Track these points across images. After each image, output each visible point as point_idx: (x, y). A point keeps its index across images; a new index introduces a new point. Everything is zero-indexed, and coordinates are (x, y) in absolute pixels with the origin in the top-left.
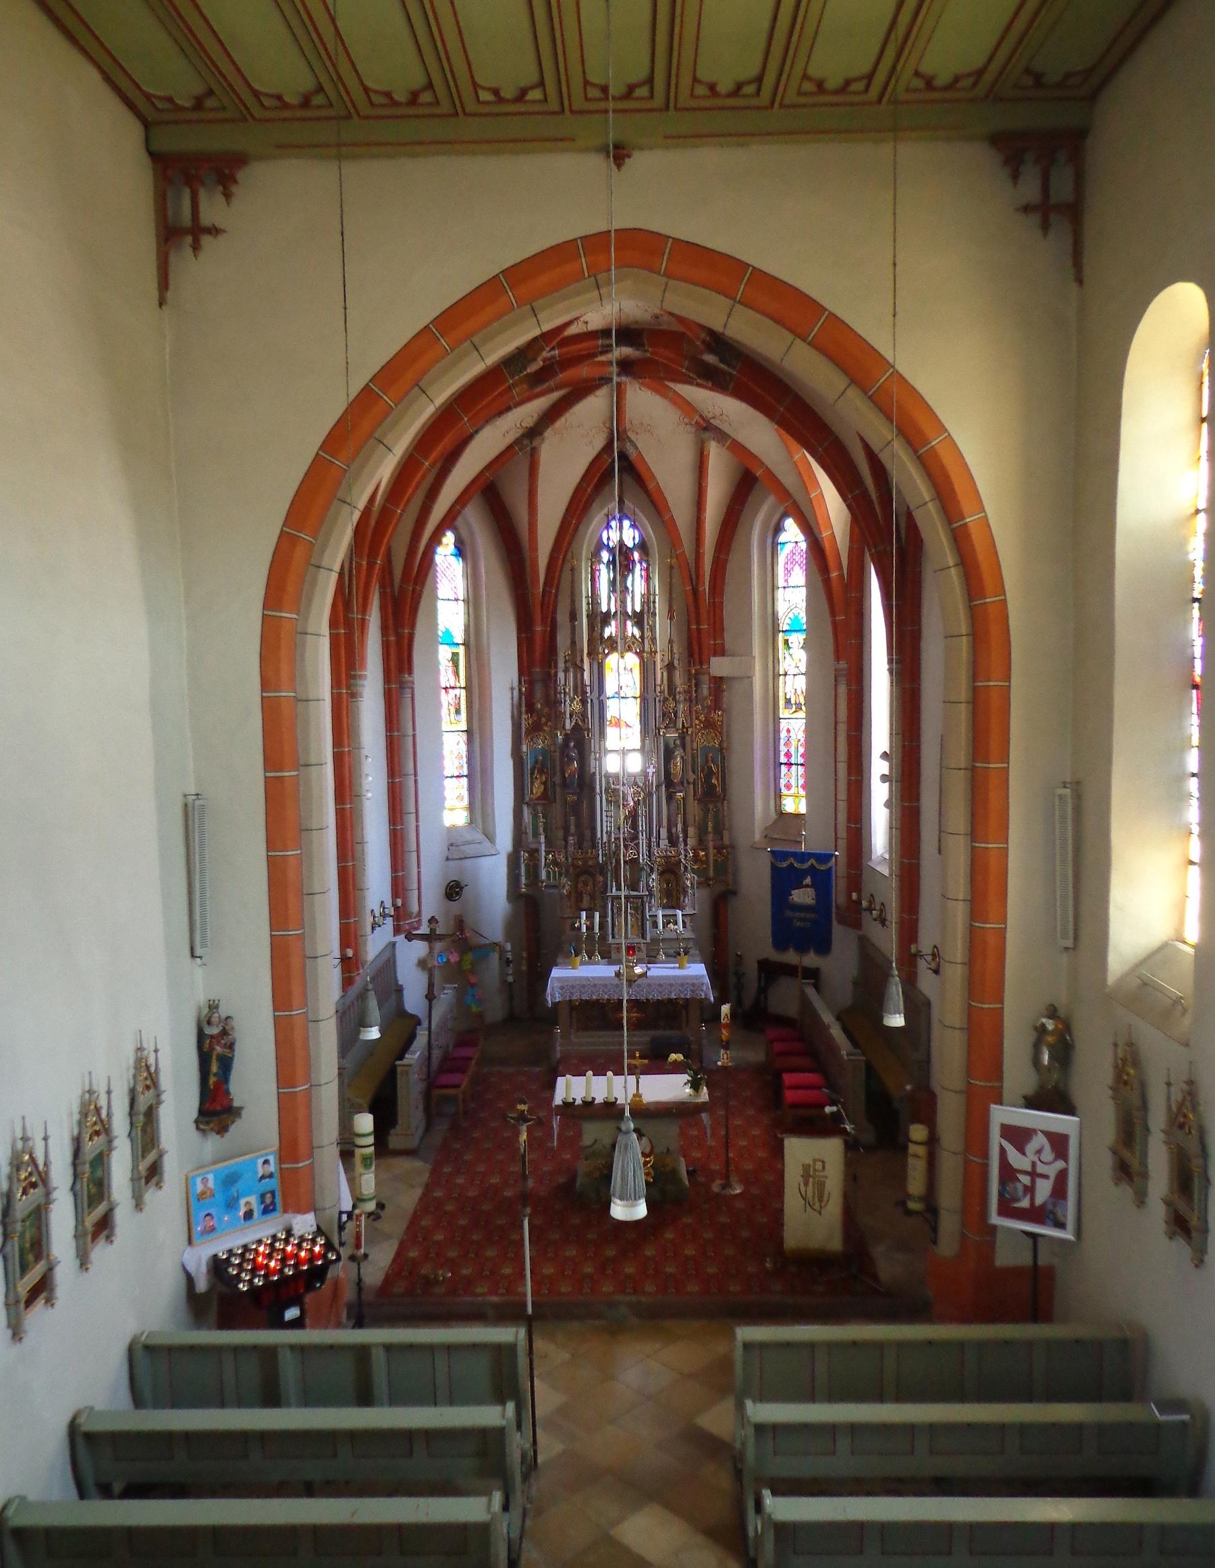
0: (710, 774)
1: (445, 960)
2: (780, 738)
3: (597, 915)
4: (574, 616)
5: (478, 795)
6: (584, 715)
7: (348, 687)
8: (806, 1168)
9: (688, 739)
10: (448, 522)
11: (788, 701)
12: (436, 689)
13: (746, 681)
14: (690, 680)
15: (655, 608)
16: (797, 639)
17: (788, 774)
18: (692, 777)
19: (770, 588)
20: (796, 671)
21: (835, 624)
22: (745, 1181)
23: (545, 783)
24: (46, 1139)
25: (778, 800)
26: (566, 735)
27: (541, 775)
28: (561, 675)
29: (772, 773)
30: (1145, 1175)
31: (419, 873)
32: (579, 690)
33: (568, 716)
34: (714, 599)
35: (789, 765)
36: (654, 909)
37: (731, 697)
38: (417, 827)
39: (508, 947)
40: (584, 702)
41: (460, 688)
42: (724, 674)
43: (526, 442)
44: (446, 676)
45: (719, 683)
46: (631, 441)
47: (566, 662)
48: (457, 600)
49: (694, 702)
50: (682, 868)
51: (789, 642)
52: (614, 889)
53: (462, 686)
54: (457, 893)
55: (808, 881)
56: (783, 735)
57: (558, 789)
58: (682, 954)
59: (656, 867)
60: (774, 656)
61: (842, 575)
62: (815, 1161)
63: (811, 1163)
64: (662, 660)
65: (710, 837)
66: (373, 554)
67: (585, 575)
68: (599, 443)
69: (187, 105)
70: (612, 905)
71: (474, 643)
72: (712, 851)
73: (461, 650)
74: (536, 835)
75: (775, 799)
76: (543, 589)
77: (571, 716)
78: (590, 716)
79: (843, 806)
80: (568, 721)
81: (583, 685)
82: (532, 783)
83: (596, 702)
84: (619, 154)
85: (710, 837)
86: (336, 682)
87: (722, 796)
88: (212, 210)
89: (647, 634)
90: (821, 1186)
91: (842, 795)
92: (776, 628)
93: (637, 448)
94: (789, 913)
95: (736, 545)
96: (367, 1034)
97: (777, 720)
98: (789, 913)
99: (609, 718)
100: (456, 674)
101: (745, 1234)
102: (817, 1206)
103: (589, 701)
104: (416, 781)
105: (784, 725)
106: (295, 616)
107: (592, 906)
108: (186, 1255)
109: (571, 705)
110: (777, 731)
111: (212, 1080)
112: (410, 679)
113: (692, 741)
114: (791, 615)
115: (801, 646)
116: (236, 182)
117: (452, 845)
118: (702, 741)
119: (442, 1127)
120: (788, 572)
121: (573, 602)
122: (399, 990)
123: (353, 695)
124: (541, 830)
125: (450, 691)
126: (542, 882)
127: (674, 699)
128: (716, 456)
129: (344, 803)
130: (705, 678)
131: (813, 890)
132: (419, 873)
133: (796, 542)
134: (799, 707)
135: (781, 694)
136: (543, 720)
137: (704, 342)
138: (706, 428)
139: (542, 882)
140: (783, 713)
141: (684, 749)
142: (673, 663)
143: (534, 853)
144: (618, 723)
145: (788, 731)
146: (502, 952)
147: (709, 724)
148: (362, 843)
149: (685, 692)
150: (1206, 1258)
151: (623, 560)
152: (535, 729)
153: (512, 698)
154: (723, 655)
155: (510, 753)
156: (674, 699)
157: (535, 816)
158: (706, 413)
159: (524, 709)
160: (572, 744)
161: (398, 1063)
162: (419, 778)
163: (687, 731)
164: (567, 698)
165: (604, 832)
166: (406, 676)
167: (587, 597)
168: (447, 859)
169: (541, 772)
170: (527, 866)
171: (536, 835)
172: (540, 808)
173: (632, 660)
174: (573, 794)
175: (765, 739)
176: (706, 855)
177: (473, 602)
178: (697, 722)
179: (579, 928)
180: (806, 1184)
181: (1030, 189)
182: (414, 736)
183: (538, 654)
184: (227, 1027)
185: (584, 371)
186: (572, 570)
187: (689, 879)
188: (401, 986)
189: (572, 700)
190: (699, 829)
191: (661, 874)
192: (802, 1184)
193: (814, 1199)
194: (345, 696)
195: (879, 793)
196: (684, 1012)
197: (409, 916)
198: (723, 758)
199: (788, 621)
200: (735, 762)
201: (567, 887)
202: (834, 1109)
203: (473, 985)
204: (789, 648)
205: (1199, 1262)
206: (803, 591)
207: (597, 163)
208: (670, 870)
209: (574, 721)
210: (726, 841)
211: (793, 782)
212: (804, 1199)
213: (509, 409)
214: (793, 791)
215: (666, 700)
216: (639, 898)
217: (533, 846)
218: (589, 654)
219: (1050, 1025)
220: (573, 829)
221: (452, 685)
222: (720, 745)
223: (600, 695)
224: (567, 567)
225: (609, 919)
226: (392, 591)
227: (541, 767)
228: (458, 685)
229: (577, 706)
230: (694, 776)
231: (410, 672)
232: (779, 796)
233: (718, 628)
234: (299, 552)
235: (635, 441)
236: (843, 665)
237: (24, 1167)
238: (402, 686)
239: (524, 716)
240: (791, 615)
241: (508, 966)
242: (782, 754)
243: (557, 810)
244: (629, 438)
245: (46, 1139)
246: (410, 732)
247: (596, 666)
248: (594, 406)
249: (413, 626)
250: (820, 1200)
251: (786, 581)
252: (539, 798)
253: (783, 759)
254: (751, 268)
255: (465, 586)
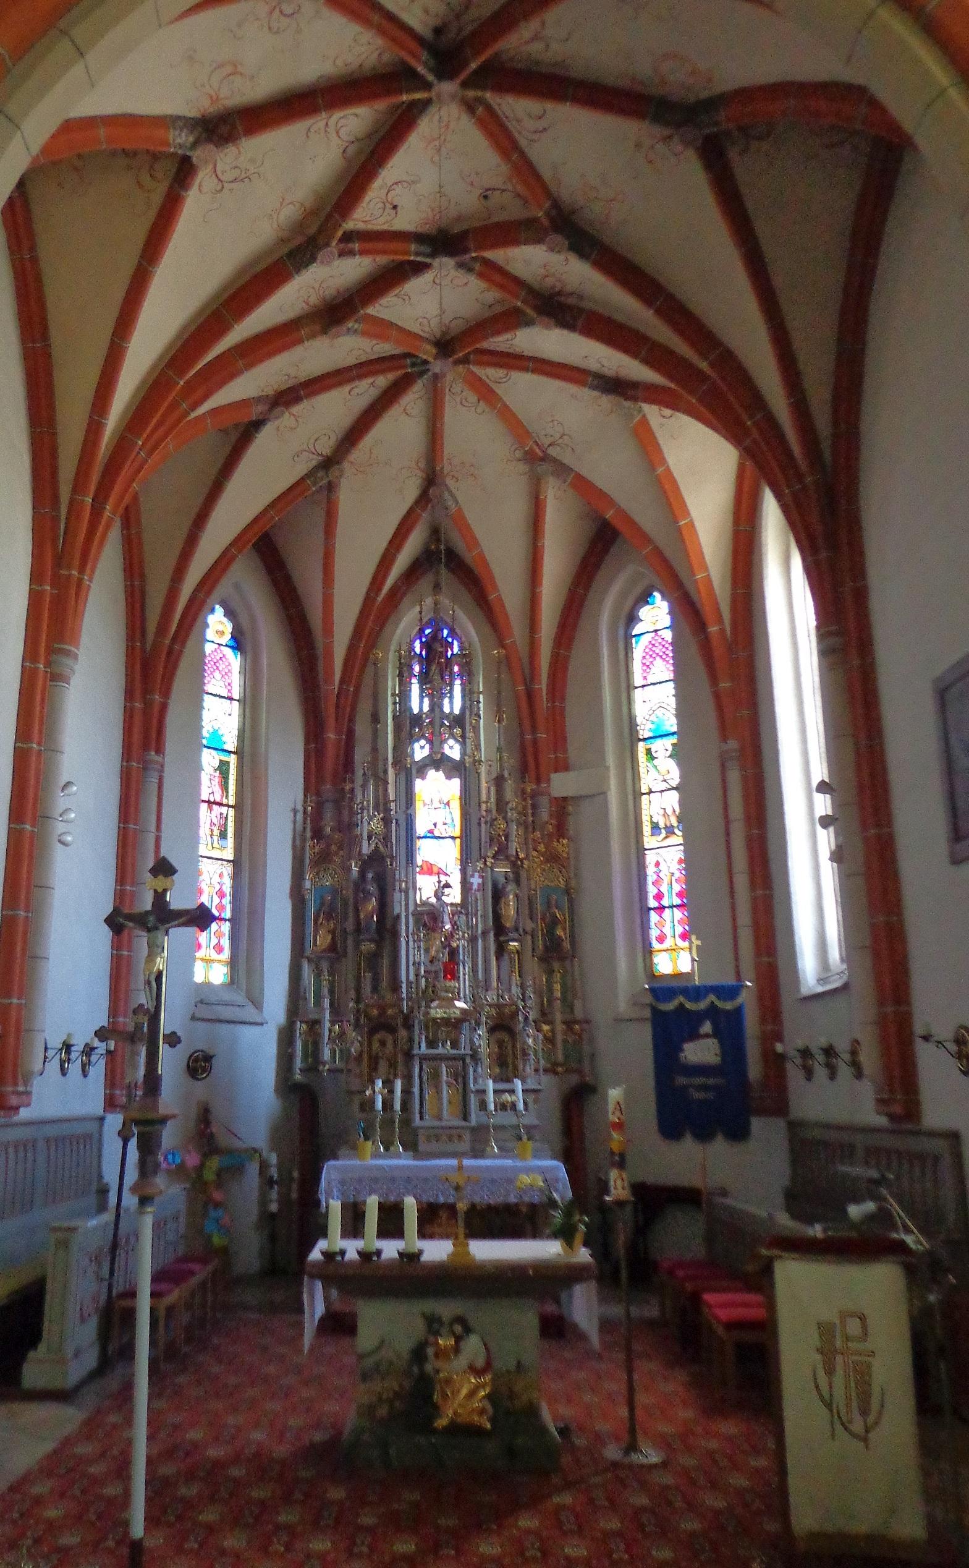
0: (555, 922)
1: (178, 1161)
2: (646, 875)
3: (398, 1085)
4: (376, 718)
5: (243, 945)
6: (386, 839)
7: (48, 664)
8: (826, 1331)
9: (523, 874)
11: (655, 828)
12: (193, 798)
15: (479, 708)
16: (663, 747)
19: (625, 688)
20: (664, 786)
21: (717, 696)
22: (664, 1443)
23: (333, 932)
27: (328, 921)
29: (638, 921)
33: (365, 837)
35: (661, 909)
36: (480, 1081)
37: (581, 821)
39: (273, 1159)
40: (386, 821)
41: (229, 806)
42: (570, 794)
43: (321, 474)
44: (209, 786)
45: (562, 806)
46: (451, 492)
48: (231, 699)
51: (653, 750)
55: (707, 1027)
56: (651, 870)
58: (525, 1138)
61: (722, 631)
62: (844, 1316)
63: (838, 1322)
64: (489, 773)
67: (392, 684)
70: (421, 1069)
72: (560, 1028)
73: (233, 760)
77: (369, 838)
78: (394, 841)
80: (365, 843)
81: (387, 801)
82: (316, 931)
90: (862, 1377)
91: (745, 918)
93: (457, 502)
94: (681, 1081)
95: (584, 624)
97: (641, 851)
98: (681, 1081)
99: (419, 863)
100: (224, 787)
101: (690, 1525)
102: (858, 1426)
103: (394, 821)
105: (650, 858)
112: (159, 759)
113: (529, 879)
115: (669, 753)
120: (647, 667)
123: (57, 678)
125: (215, 807)
126: (324, 1064)
130: (544, 801)
131: (715, 1041)
133: (656, 631)
134: (670, 831)
135: (645, 819)
136: (334, 848)
139: (324, 1064)
140: (649, 841)
143: (314, 1025)
145: (657, 864)
146: (264, 1166)
148: (45, 887)
151: (437, 1013)
152: (322, 860)
153: (295, 822)
155: (288, 891)
156: (505, 818)
157: (318, 976)
159: (309, 834)
160: (370, 875)
163: (522, 863)
165: (411, 964)
166: (153, 753)
167: (393, 695)
168: (193, 1018)
169: (329, 916)
172: (325, 965)
173: (452, 788)
174: (369, 940)
176: (553, 1031)
177: (250, 703)
178: (535, 854)
179: (372, 1101)
180: (830, 1371)
187: (531, 1039)
189: (371, 819)
191: (492, 1030)
192: (821, 1373)
193: (848, 1405)
194: (41, 675)
198: (571, 902)
199: (649, 726)
200: (587, 908)
202: (870, 1206)
203: (217, 1205)
204: (654, 758)
206: (670, 688)
210: (579, 1013)
211: (667, 930)
212: (829, 1405)
214: (669, 943)
217: (316, 1017)
218: (394, 764)
221: (218, 800)
223: (407, 808)
227: (329, 912)
228: (225, 801)
229: (376, 825)
230: (533, 926)
231: (159, 750)
232: (648, 952)
233: (559, 739)
236: (733, 744)
239: (309, 843)
240: (653, 718)
241: (272, 1187)
242: (651, 896)
243: (348, 966)
249: (166, 693)
250: (864, 1412)
251: (645, 678)
252: (324, 951)
253: (652, 903)
255: (242, 683)
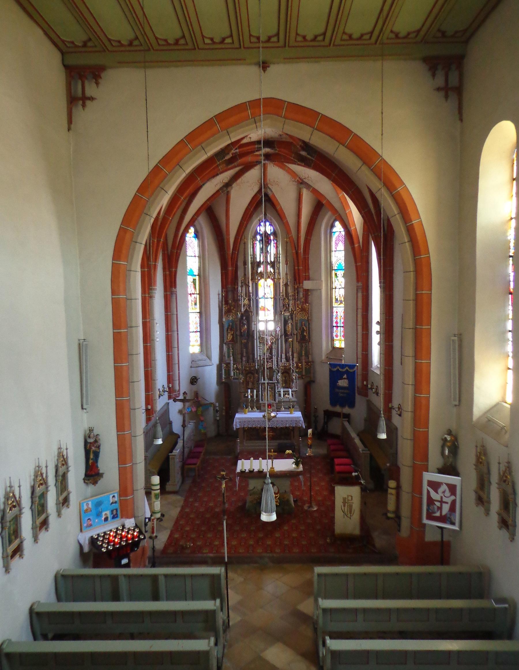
0: (303, 331)
1: (190, 410)
2: (333, 316)
3: (255, 391)
4: (245, 263)
5: (204, 340)
6: (249, 306)
7: (149, 294)
8: (344, 499)
9: (294, 316)
10: (191, 223)
11: (337, 300)
12: (186, 294)
13: (319, 291)
14: (295, 290)
15: (280, 260)
16: (340, 273)
17: (337, 331)
18: (295, 332)
19: (329, 251)
20: (340, 287)
21: (357, 267)
22: (318, 505)
23: (233, 335)
24: (19, 487)
25: (332, 342)
26: (242, 314)
27: (231, 331)
28: (240, 288)
29: (330, 330)
30: (489, 502)
31: (179, 373)
32: (247, 295)
33: (243, 306)
34: (305, 256)
35: (337, 327)
36: (279, 388)
37: (312, 298)
38: (178, 353)
39: (217, 404)
40: (249, 300)
41: (197, 294)
42: (309, 288)
43: (225, 189)
44: (190, 289)
45: (307, 292)
46: (270, 188)
47: (242, 283)
48: (195, 256)
49: (296, 300)
50: (291, 371)
51: (337, 274)
52: (262, 380)
53: (198, 293)
54: (195, 382)
55: (345, 376)
56: (335, 314)
57: (238, 337)
58: (292, 408)
59: (280, 370)
60: (330, 280)
61: (359, 246)
62: (348, 496)
63: (347, 497)
64: (283, 282)
65: (303, 358)
66: (159, 237)
67: (250, 246)
68: (256, 189)
69: (80, 45)
70: (262, 387)
71: (202, 275)
72: (304, 364)
73: (197, 278)
74: (229, 357)
75: (331, 341)
76: (232, 252)
77: (244, 306)
78: (252, 306)
79: (360, 344)
80: (242, 308)
81: (249, 293)
82: (227, 335)
83: (255, 300)
84: (264, 66)
85: (303, 358)
86: (144, 292)
87: (308, 340)
88: (91, 90)
89: (277, 271)
90: (351, 507)
91: (360, 340)
92: (332, 268)
93: (272, 191)
94: (337, 390)
95: (315, 233)
96: (157, 442)
97: (332, 307)
98: (337, 390)
99: (260, 307)
100: (195, 288)
101: (318, 527)
102: (349, 515)
103: (252, 299)
104: (178, 334)
105: (335, 310)
106: (126, 263)
107: (253, 387)
108: (79, 536)
109: (244, 301)
110: (332, 312)
111: (91, 461)
112: (175, 290)
113: (296, 317)
114: (338, 263)
115: (342, 276)
116: (101, 78)
117: (193, 361)
118: (300, 317)
119: (189, 482)
120: (337, 244)
121: (245, 257)
122: (171, 423)
123: (151, 297)
124: (231, 355)
125: (192, 295)
126: (232, 377)
127: (288, 299)
128: (306, 195)
129: (147, 343)
130: (301, 290)
131: (347, 380)
132: (179, 373)
133: (340, 232)
134: (341, 302)
135: (334, 297)
136: (232, 308)
137: (301, 146)
138: (301, 183)
139: (232, 377)
140: (335, 305)
141: (292, 320)
142: (287, 283)
143: (228, 364)
144: (264, 309)
145: (337, 312)
146: (215, 407)
147: (303, 310)
148: (155, 360)
149: (293, 296)
150: (515, 538)
151: (266, 239)
152: (229, 311)
153: (219, 298)
154: (309, 280)
155: (218, 322)
156: (288, 299)
157: (228, 349)
158: (302, 177)
159: (224, 303)
160: (244, 318)
161: (170, 454)
162: (179, 333)
163: (294, 312)
164: (242, 298)
165: (258, 356)
166: (174, 289)
167: (251, 255)
168: (191, 367)
169: (231, 330)
170: (225, 370)
171: (229, 357)
172: (230, 345)
173: (270, 282)
174: (245, 339)
175: (327, 316)
176: (302, 365)
177: (202, 257)
178: (298, 309)
179: (248, 397)
180: (344, 506)
181: (440, 81)
182: (177, 314)
183: (230, 280)
184: (97, 439)
185: (249, 159)
186: (245, 243)
187: (294, 376)
188: (171, 421)
189: (244, 299)
190: (299, 354)
191: (282, 373)
192: (343, 506)
193: (348, 512)
194: (147, 297)
195: (376, 339)
196: (292, 432)
197: (175, 391)
198: (309, 324)
199: (336, 265)
200: (314, 326)
201: (242, 379)
202: (356, 474)
203: (202, 421)
204: (337, 277)
205: (512, 539)
206: (343, 252)
207: (255, 70)
208: (286, 372)
209: (245, 308)
210: (310, 359)
211: (339, 334)
212: (344, 512)
213: (217, 175)
214: (339, 338)
215: (284, 299)
216: (273, 384)
217: (228, 362)
218: (252, 280)
219: (449, 438)
220: (245, 354)
221: (193, 293)
222: (307, 318)
223: (256, 297)
224: (242, 242)
225: (260, 393)
226: (168, 253)
227: (231, 328)
228: (196, 293)
229: (246, 302)
230: (296, 332)
231: (175, 287)
232: (333, 340)
233: (307, 268)
234: (128, 236)
235: (271, 189)
236: (360, 284)
237: (10, 498)
238: (172, 293)
239: (224, 306)
240: (338, 263)
241: (217, 413)
242: (334, 322)
243: (238, 346)
244: (269, 187)
245: (19, 487)
246: (175, 313)
247: (254, 285)
248: (254, 174)
249: (176, 267)
250: (350, 513)
251: (336, 248)
252: (230, 341)
253: (334, 325)
254: (321, 115)
255: (199, 250)
